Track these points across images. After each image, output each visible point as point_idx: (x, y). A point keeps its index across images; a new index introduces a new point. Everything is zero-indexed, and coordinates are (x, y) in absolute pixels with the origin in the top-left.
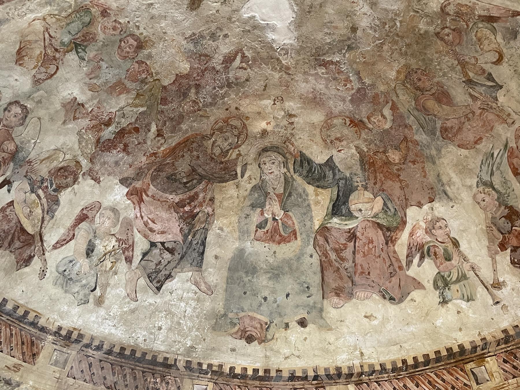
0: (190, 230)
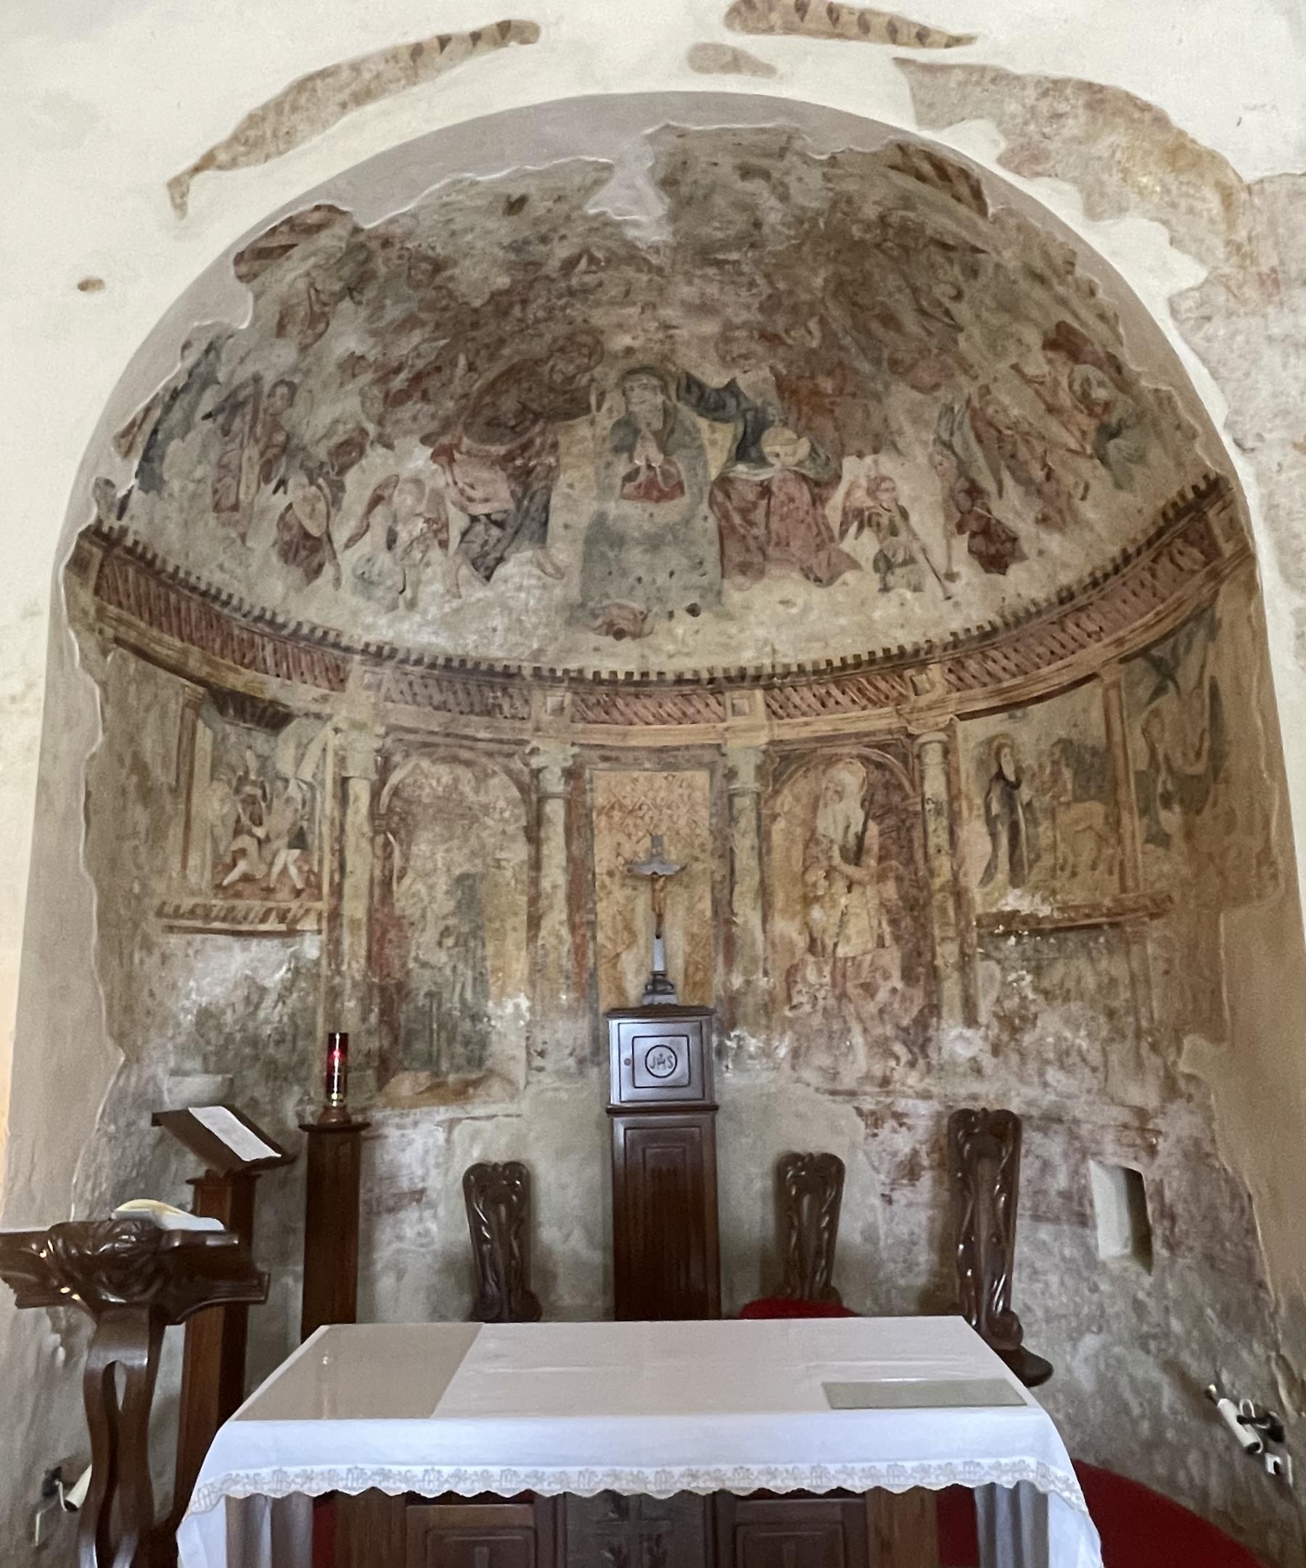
0: (525, 493)
